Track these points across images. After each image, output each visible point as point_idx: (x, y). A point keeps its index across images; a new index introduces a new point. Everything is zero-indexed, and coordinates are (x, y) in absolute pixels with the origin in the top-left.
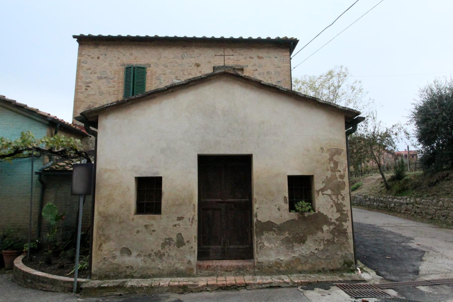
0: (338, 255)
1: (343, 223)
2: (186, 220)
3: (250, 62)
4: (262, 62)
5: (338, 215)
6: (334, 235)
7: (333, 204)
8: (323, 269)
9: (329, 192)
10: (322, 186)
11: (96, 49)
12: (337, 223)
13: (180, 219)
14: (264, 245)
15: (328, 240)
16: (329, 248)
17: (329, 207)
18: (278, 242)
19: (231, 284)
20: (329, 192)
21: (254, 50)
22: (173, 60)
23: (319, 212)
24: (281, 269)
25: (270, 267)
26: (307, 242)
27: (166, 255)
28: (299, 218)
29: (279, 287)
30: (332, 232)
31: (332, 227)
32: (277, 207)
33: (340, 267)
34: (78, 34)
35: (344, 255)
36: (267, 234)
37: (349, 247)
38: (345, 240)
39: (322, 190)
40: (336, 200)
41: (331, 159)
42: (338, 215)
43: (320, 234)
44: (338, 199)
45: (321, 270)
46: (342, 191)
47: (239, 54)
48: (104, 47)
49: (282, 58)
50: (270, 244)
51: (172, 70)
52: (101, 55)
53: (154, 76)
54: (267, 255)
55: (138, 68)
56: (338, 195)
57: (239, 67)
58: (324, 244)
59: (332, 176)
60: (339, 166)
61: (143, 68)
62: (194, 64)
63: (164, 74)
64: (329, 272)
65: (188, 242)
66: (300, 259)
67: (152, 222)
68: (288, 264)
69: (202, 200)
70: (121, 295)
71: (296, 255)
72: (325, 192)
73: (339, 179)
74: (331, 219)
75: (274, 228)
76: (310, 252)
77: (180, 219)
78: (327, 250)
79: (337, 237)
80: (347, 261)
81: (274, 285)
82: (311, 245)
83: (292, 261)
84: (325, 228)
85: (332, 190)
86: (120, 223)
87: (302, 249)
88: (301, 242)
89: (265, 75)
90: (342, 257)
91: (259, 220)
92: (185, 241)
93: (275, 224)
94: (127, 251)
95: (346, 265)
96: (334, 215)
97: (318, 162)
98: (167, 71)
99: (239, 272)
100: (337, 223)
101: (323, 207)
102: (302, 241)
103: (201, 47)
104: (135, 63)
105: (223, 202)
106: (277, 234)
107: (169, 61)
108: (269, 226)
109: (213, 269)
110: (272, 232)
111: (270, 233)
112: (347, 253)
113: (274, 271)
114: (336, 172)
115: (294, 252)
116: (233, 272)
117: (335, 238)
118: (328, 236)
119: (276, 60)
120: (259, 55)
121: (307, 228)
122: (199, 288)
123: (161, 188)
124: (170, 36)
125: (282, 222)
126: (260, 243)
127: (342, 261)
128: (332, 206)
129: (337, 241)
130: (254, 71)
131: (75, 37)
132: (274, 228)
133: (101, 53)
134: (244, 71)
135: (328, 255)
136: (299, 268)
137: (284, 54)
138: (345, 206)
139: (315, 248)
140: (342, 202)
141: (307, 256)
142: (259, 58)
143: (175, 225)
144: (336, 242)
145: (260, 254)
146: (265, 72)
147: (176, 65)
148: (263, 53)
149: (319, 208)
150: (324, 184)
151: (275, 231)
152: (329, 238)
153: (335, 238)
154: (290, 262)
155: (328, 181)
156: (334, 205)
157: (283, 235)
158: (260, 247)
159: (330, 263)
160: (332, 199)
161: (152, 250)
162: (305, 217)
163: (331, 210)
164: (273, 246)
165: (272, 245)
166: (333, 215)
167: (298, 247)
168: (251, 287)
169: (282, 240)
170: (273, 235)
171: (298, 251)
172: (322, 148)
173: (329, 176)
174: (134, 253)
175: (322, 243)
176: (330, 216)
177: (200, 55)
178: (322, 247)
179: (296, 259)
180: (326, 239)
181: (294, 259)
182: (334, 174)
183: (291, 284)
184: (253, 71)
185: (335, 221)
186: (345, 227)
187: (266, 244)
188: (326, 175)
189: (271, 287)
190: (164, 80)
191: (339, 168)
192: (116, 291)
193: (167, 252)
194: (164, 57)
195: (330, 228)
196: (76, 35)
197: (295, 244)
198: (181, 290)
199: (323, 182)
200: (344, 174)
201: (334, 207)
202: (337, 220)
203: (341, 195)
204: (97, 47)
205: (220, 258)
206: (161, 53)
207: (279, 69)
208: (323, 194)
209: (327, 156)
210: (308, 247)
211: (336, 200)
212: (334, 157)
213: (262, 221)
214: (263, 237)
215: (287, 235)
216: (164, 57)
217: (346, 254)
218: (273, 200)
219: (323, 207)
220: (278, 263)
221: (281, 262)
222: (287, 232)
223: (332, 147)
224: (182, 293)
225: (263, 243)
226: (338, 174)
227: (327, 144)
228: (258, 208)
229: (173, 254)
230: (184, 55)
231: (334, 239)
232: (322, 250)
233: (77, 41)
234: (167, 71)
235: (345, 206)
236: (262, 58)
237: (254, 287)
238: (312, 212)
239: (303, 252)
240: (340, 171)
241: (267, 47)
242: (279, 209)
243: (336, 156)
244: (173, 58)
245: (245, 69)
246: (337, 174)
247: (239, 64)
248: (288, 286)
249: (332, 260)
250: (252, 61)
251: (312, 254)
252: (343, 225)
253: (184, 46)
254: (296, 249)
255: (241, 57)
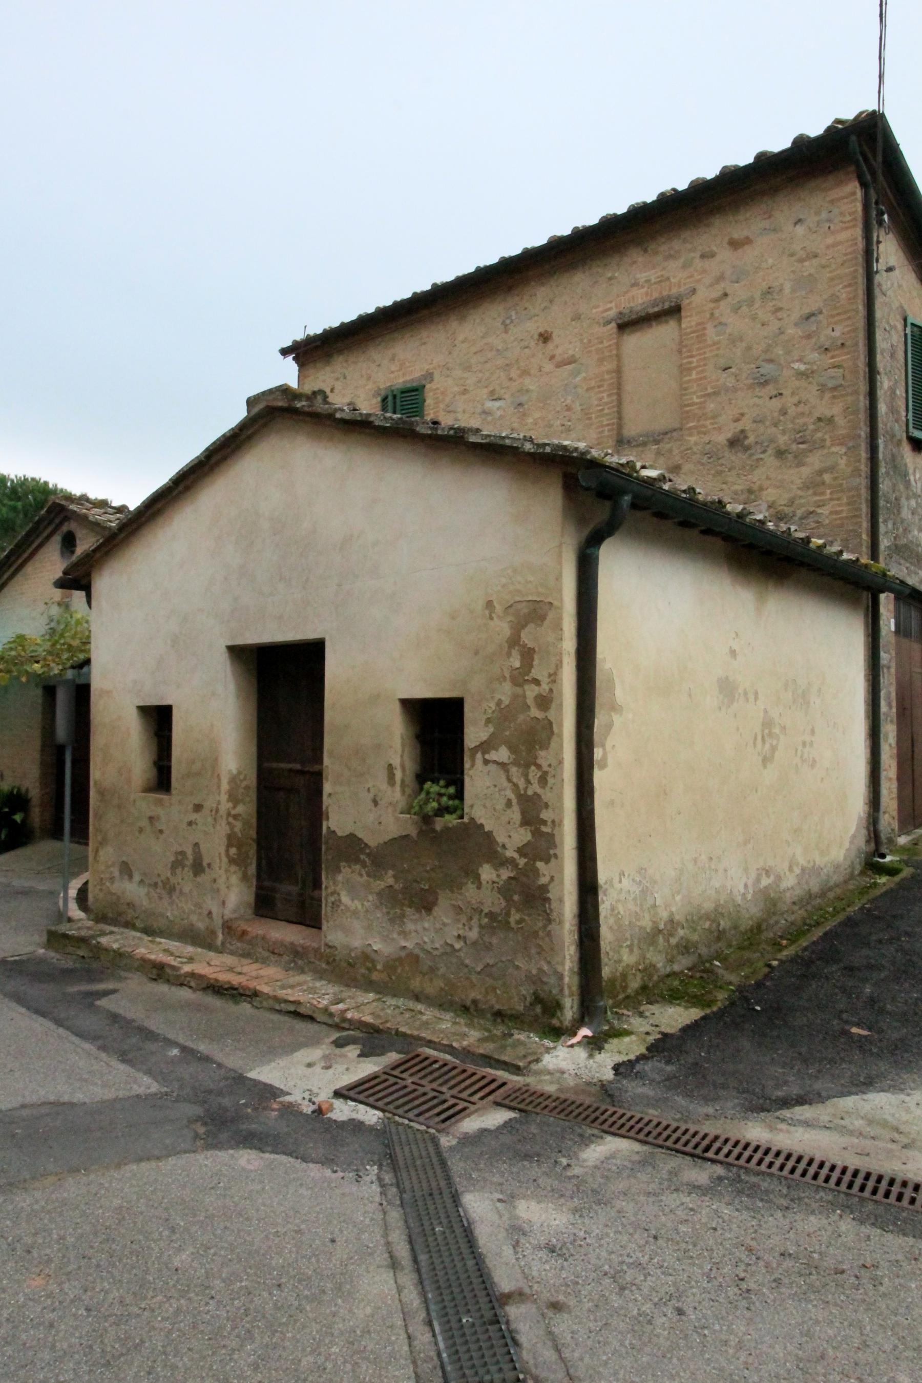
0: (518, 968)
1: (540, 865)
2: (206, 811)
3: (704, 271)
4: (749, 255)
5: (522, 836)
6: (509, 899)
7: (512, 796)
8: (475, 1002)
9: (502, 754)
10: (484, 735)
11: (328, 369)
12: (522, 862)
13: (198, 808)
14: (340, 901)
15: (491, 915)
16: (495, 941)
17: (500, 806)
18: (370, 898)
19: (229, 982)
20: (502, 754)
21: (717, 221)
22: (485, 341)
23: (472, 819)
24: (375, 976)
25: (349, 964)
26: (437, 911)
27: (178, 891)
28: (421, 833)
29: (311, 1018)
30: (505, 891)
31: (506, 874)
32: (371, 795)
33: (521, 1008)
34: (288, 343)
35: (534, 972)
36: (348, 870)
37: (552, 949)
38: (540, 924)
39: (485, 747)
40: (522, 784)
41: (514, 641)
42: (522, 836)
43: (470, 891)
44: (528, 782)
45: (468, 1003)
46: (542, 753)
47: (670, 257)
48: (341, 358)
49: (824, 215)
50: (353, 900)
51: (480, 375)
52: (337, 379)
53: (442, 406)
54: (347, 931)
55: (403, 392)
56: (527, 766)
57: (667, 306)
58: (481, 926)
59: (515, 697)
60: (535, 663)
61: (416, 390)
62: (536, 337)
63: (465, 392)
64: (489, 1016)
65: (209, 865)
66: (417, 957)
67: (160, 811)
68: (392, 965)
69: (266, 765)
70: (83, 957)
71: (409, 945)
72: (493, 756)
73: (535, 712)
74: (504, 846)
75: (362, 857)
76: (442, 942)
77: (198, 808)
78: (488, 947)
79: (518, 910)
80: (542, 995)
81: (302, 1010)
82: (446, 921)
83: (400, 960)
84: (487, 873)
85: (513, 749)
86: (119, 807)
87: (425, 929)
88: (424, 907)
89: (758, 304)
90: (529, 978)
91: (332, 829)
92: (205, 864)
93: (366, 845)
94: (126, 870)
95: (538, 1009)
96: (515, 836)
97: (476, 653)
98: (471, 380)
99: (294, 961)
100: (522, 862)
101: (485, 806)
102: (426, 905)
103: (551, 273)
104: (401, 381)
105: (301, 772)
106: (368, 875)
107: (474, 349)
108: (352, 848)
109: (250, 942)
110: (358, 867)
111: (353, 867)
112: (546, 968)
113: (359, 977)
114: (526, 687)
115: (404, 934)
116: (286, 958)
117: (513, 911)
118: (491, 901)
119: (800, 230)
120: (735, 236)
121: (441, 867)
122: (178, 976)
123: (170, 730)
124: (488, 264)
125: (382, 842)
126: (332, 894)
127: (526, 990)
128: (509, 804)
129: (518, 922)
130: (717, 300)
131: (285, 352)
132: (362, 857)
133: (336, 375)
134: (683, 314)
135: (491, 962)
136: (416, 984)
137: (834, 194)
138: (547, 806)
139: (456, 934)
140: (540, 791)
141: (435, 953)
142: (735, 244)
143: (190, 824)
144: (513, 924)
145: (331, 923)
146: (758, 295)
147: (490, 355)
148: (749, 223)
149: (472, 806)
150: (491, 729)
151: (364, 865)
152: (496, 909)
153: (513, 911)
154: (395, 960)
155: (504, 715)
156: (515, 801)
157: (380, 878)
158: (333, 903)
159: (494, 989)
160: (509, 780)
161: (159, 875)
162: (434, 830)
163: (504, 819)
164: (360, 907)
165: (356, 902)
166: (511, 836)
167: (415, 921)
168: (261, 1002)
169: (380, 894)
170: (361, 875)
171: (413, 934)
172: (489, 604)
173: (506, 701)
174: (137, 877)
175: (475, 922)
176: (500, 838)
177: (551, 302)
178: (473, 935)
179: (408, 956)
180: (486, 911)
181: (403, 954)
182: (519, 690)
183: (337, 1020)
184: (712, 305)
185: (516, 855)
186: (543, 880)
187: (345, 899)
188: (498, 696)
189: (296, 1014)
190: (464, 412)
191: (535, 673)
192: (79, 948)
193: (178, 884)
194: (463, 342)
195: (498, 876)
196: (285, 346)
197: (408, 911)
198: (155, 971)
199: (488, 721)
200: (551, 690)
201: (516, 808)
202: (521, 851)
203: (539, 767)
204: (328, 363)
205: (295, 920)
206: (454, 333)
207: (810, 267)
208: (486, 762)
209: (502, 628)
210: (438, 926)
211: (522, 784)
212: (522, 635)
213: (340, 834)
214: (340, 878)
215: (390, 881)
216: (463, 342)
217: (540, 970)
218: (362, 775)
219: (485, 806)
220: (367, 958)
221: (373, 956)
222: (391, 872)
223: (518, 599)
224: (155, 980)
225: (339, 894)
226: (531, 692)
227: (504, 586)
228: (330, 794)
229: (186, 889)
230: (510, 317)
231: (508, 914)
232: (474, 943)
233: (294, 359)
234: (471, 380)
235: (547, 806)
236: (748, 241)
237: (265, 1004)
238: (450, 820)
239: (426, 939)
240: (537, 682)
241: (763, 193)
242: (375, 802)
243: (531, 627)
244: (483, 337)
245: (685, 303)
246: (528, 693)
247: (665, 293)
248: (330, 1022)
249: (500, 982)
250: (712, 266)
251: (448, 949)
252: (537, 870)
253: (510, 288)
254: (410, 926)
255: (673, 265)
